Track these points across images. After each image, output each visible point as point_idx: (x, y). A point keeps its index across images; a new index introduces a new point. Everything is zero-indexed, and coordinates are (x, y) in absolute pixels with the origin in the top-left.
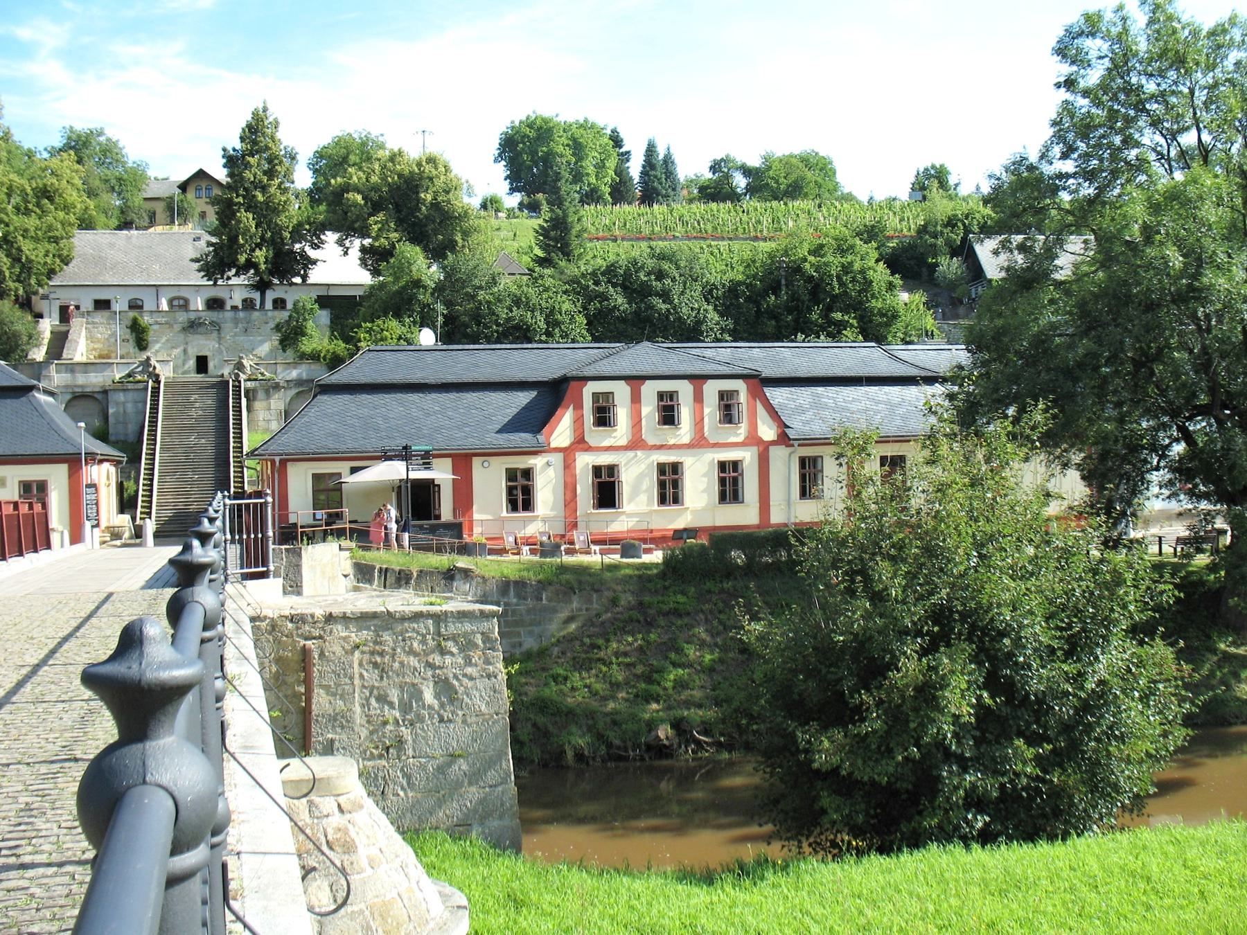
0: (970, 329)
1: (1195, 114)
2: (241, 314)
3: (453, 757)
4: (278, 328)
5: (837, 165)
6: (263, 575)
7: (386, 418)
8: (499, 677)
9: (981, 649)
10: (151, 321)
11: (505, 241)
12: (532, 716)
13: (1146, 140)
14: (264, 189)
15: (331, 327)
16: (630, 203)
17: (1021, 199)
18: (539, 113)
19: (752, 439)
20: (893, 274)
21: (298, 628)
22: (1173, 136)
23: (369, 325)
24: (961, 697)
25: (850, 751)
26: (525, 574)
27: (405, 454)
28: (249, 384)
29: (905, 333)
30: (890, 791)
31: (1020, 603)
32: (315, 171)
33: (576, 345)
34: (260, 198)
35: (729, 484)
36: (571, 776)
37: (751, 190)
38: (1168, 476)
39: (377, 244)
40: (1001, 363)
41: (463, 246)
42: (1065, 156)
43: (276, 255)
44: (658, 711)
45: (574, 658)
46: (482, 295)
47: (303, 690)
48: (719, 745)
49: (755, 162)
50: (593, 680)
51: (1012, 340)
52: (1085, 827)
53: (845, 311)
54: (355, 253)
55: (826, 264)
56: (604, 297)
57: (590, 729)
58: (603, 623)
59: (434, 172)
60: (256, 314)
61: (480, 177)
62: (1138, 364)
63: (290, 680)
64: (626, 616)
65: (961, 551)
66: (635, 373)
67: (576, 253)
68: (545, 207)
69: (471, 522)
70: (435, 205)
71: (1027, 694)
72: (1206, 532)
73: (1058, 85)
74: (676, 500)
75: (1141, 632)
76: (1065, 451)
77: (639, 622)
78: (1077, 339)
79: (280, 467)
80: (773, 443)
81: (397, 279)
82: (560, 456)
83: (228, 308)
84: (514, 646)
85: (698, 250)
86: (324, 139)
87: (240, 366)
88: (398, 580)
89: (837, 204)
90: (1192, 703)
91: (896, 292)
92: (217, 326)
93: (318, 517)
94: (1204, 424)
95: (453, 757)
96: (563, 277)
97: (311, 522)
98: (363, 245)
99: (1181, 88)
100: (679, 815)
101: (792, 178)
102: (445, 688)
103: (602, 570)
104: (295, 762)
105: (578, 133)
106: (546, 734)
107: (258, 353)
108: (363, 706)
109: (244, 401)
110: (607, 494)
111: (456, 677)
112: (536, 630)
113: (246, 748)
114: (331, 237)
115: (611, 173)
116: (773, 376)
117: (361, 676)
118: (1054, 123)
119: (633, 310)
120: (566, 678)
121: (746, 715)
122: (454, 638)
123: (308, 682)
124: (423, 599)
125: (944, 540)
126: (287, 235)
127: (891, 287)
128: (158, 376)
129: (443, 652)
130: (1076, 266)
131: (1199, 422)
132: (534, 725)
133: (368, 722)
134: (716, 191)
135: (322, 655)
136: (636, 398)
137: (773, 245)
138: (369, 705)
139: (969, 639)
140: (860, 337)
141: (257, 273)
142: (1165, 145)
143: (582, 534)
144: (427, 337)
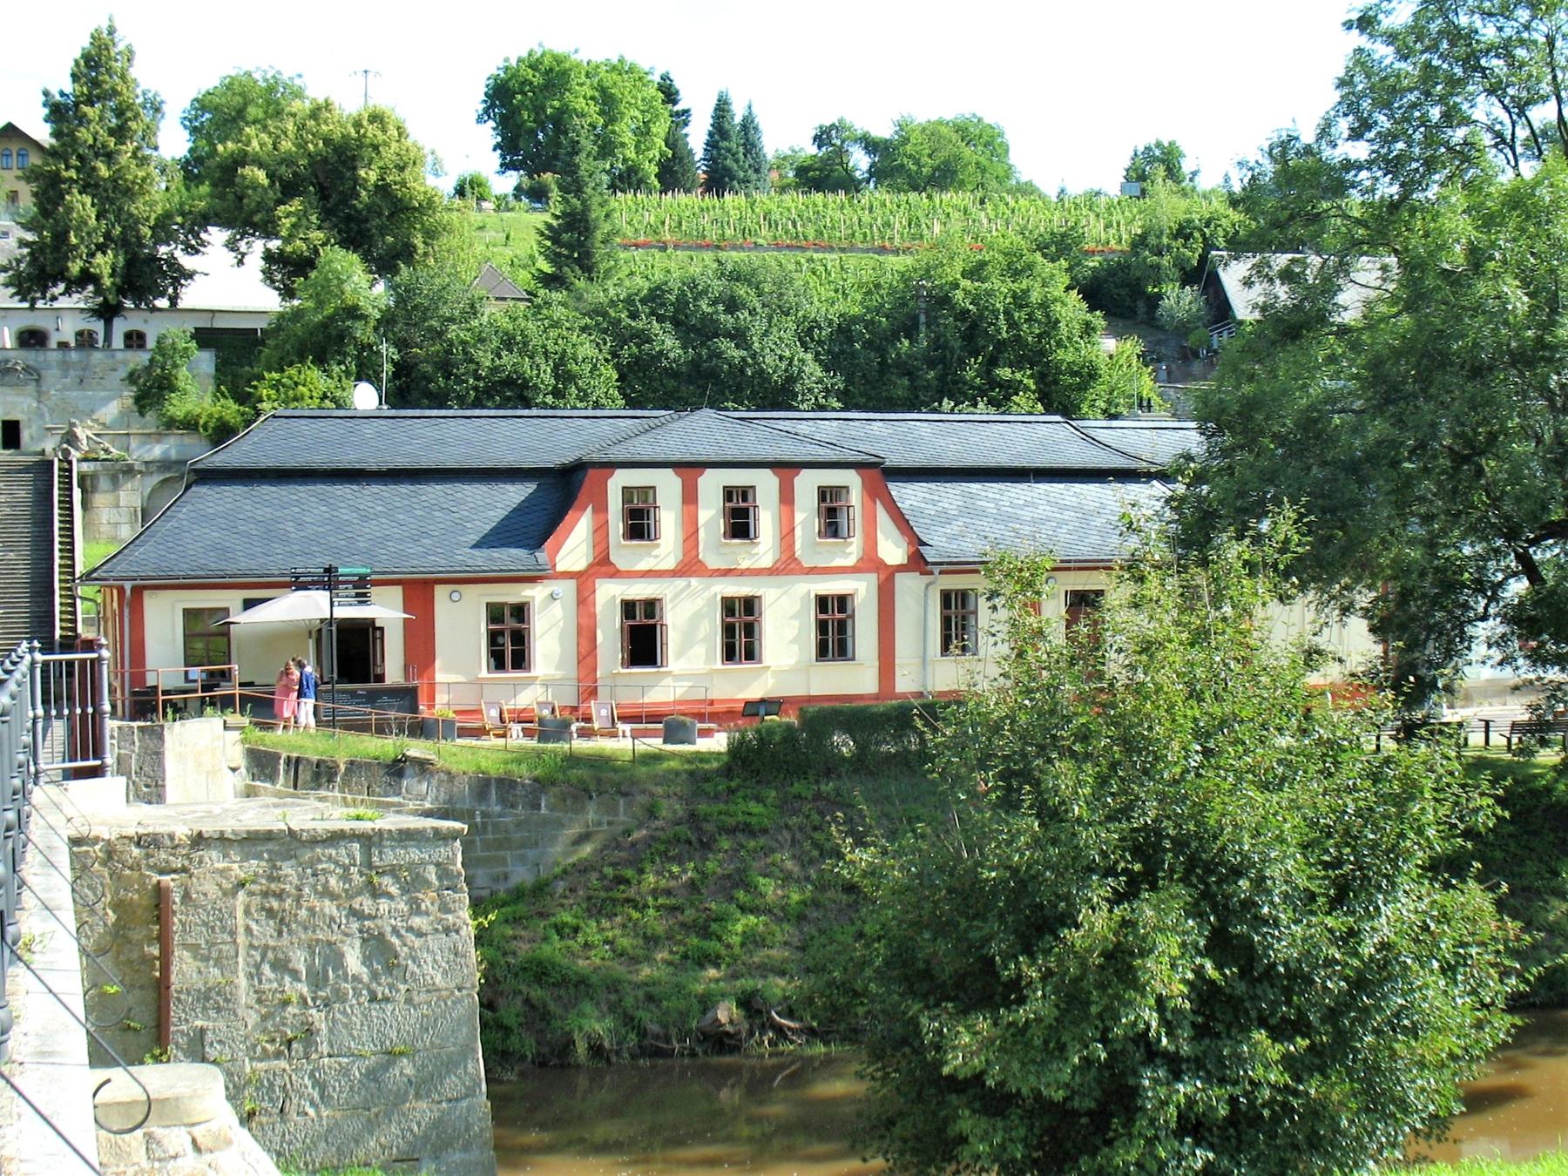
0: (1204, 399)
1: (1555, 77)
2: (74, 356)
3: (392, 1056)
4: (132, 378)
5: (1011, 138)
6: (95, 772)
7: (300, 524)
8: (463, 932)
9: (1206, 895)
11: (491, 245)
12: (523, 988)
13: (1478, 114)
14: (110, 157)
15: (217, 378)
16: (687, 191)
17: (1291, 200)
18: (547, 46)
19: (870, 562)
20: (1092, 309)
21: (148, 856)
22: (1520, 108)
23: (275, 375)
24: (1171, 968)
25: (1000, 1049)
26: (514, 767)
27: (328, 580)
28: (85, 467)
29: (1109, 402)
30: (1062, 1111)
31: (1268, 828)
32: (194, 131)
33: (598, 413)
34: (104, 171)
35: (832, 630)
36: (582, 1081)
37: (878, 174)
38: (1501, 630)
39: (289, 249)
40: (1251, 451)
41: (426, 254)
42: (1356, 135)
43: (130, 263)
44: (717, 981)
45: (589, 898)
46: (453, 332)
47: (156, 952)
48: (812, 1032)
49: (883, 130)
50: (617, 932)
51: (1267, 418)
52: (1356, 1164)
53: (1016, 365)
54: (255, 261)
55: (990, 293)
56: (643, 337)
57: (612, 1008)
58: (633, 845)
59: (381, 137)
60: (97, 356)
61: (453, 147)
62: (1459, 459)
63: (136, 935)
64: (670, 833)
65: (1175, 745)
66: (688, 458)
67: (603, 266)
68: (555, 194)
69: (432, 686)
70: (383, 189)
71: (1273, 966)
72: (1556, 715)
73: (1348, 25)
74: (750, 655)
75: (1446, 869)
76: (1346, 588)
77: (689, 843)
78: (1366, 417)
79: (132, 599)
80: (901, 568)
81: (320, 304)
82: (571, 584)
83: (53, 345)
84: (496, 880)
85: (792, 267)
86: (207, 80)
87: (71, 439)
88: (317, 776)
89: (1009, 199)
90: (1520, 976)
91: (1096, 338)
92: (34, 374)
93: (191, 677)
94: (1557, 551)
95: (392, 1056)
96: (581, 305)
97: (181, 684)
98: (268, 250)
99: (1535, 36)
100: (751, 1140)
101: (942, 155)
102: (378, 948)
103: (633, 761)
104: (117, 1074)
105: (609, 80)
106: (546, 1016)
107: (100, 419)
108: (250, 976)
109: (77, 494)
110: (643, 643)
111: (395, 931)
112: (531, 854)
113: (44, 1055)
114: (216, 236)
115: (660, 143)
116: (904, 464)
117: (248, 930)
118: (1342, 83)
119: (690, 362)
120: (576, 930)
121: (846, 992)
122: (393, 871)
123: (164, 940)
124: (346, 811)
125: (1150, 728)
126: (146, 231)
127: (1088, 329)
129: (376, 893)
130: (1368, 304)
131: (1550, 547)
132: (527, 1001)
133: (259, 1001)
134: (822, 175)
135: (186, 896)
136: (690, 497)
137: (909, 260)
138: (260, 975)
139: (1185, 880)
140: (1040, 407)
141: (99, 291)
142: (1507, 121)
143: (603, 705)
144: (365, 397)
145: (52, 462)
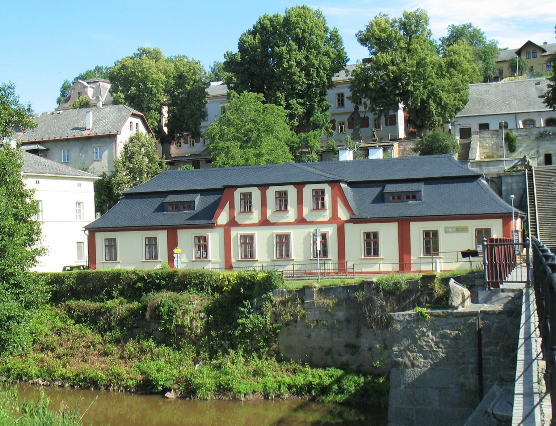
10: (517, 135)
36: (270, 401)
128: (531, 167)
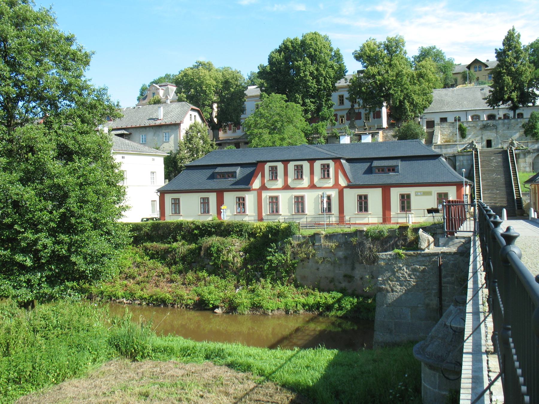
4: (523, 126)
10: (467, 126)
28: (516, 151)
34: (514, 70)
80: (346, 187)
83: (497, 119)
87: (512, 144)
92: (495, 127)
107: (516, 138)
126: (526, 85)
128: (476, 149)
145: (507, 151)
